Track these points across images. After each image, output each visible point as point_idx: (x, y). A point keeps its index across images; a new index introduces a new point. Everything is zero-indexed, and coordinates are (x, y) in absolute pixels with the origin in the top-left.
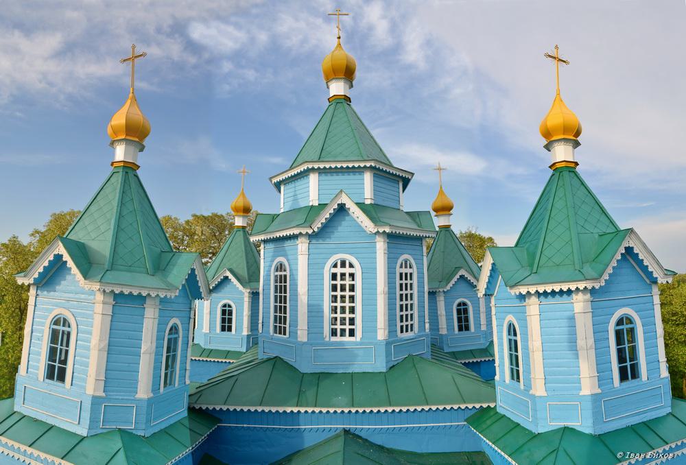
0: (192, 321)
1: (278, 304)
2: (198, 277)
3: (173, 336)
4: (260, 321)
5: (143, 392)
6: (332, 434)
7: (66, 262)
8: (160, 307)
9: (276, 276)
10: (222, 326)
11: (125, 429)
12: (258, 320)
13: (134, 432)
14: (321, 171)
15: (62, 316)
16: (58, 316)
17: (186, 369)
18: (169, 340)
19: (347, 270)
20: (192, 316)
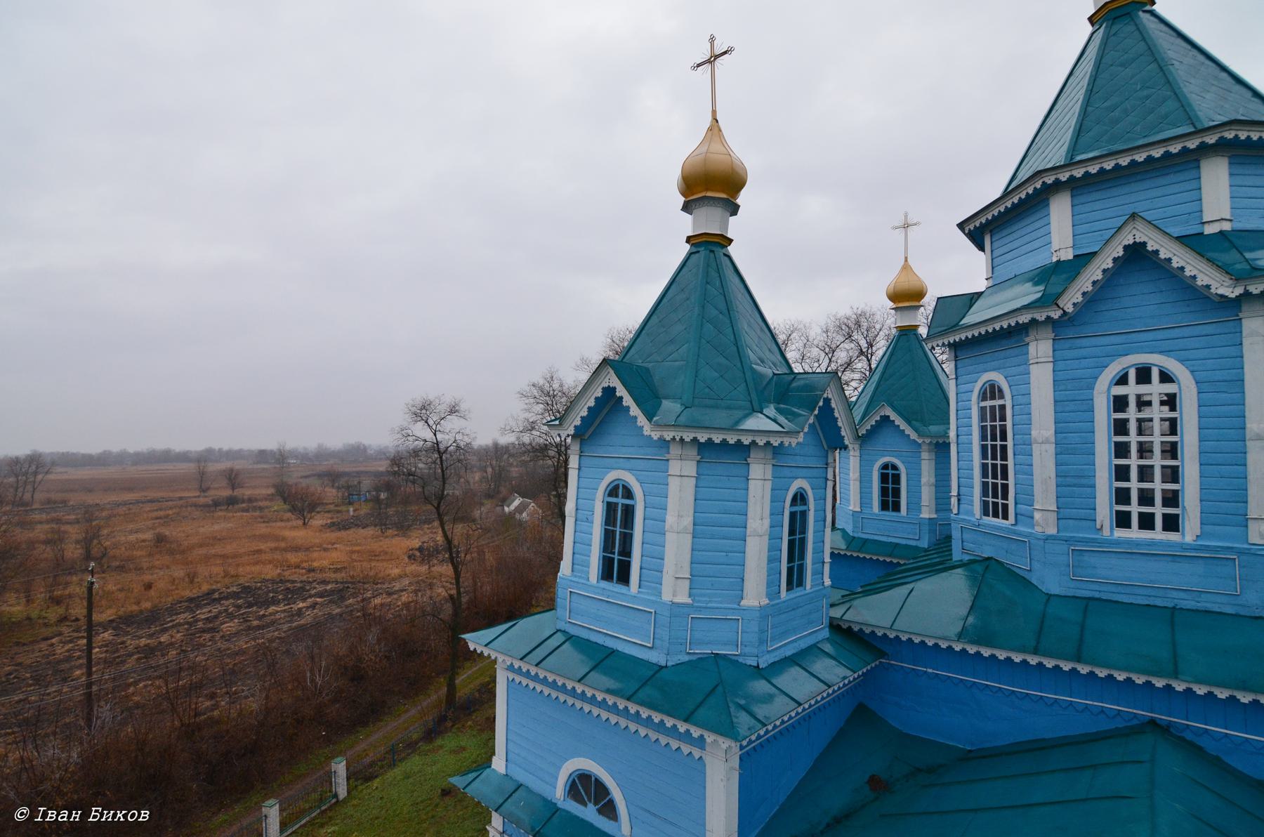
0: (830, 484)
1: (990, 480)
2: (836, 411)
3: (799, 508)
4: (954, 492)
5: (755, 595)
6: (1120, 724)
7: (621, 398)
8: (774, 462)
9: (983, 409)
10: (882, 488)
11: (725, 655)
12: (950, 486)
13: (741, 660)
14: (1074, 186)
15: (621, 483)
16: (616, 483)
17: (823, 562)
18: (793, 515)
19: (1156, 389)
20: (830, 476)
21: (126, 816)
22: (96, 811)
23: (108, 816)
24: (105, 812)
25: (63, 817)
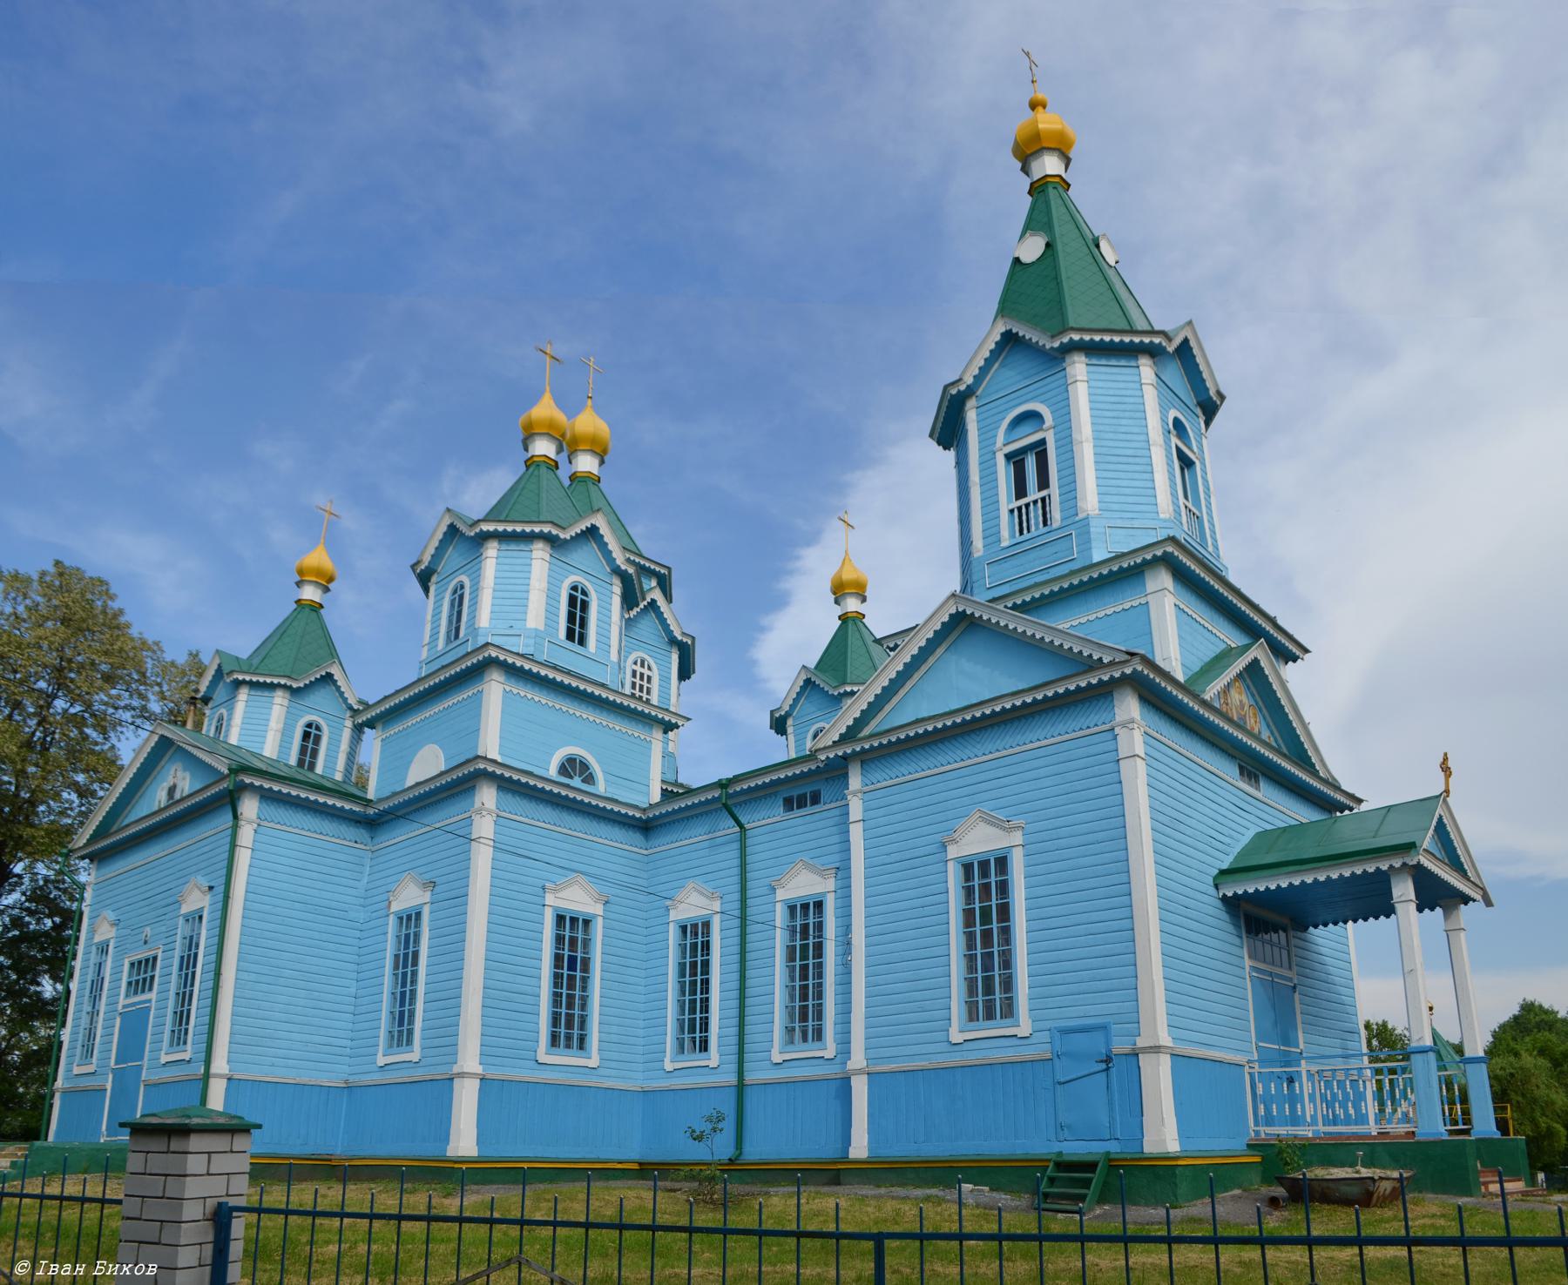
22: (101, 1265)
23: (113, 1269)
25: (66, 1271)
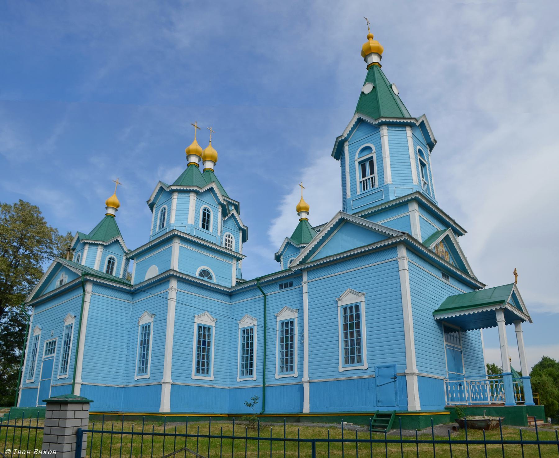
21: (47, 453)
23: (40, 452)
24: (40, 451)
